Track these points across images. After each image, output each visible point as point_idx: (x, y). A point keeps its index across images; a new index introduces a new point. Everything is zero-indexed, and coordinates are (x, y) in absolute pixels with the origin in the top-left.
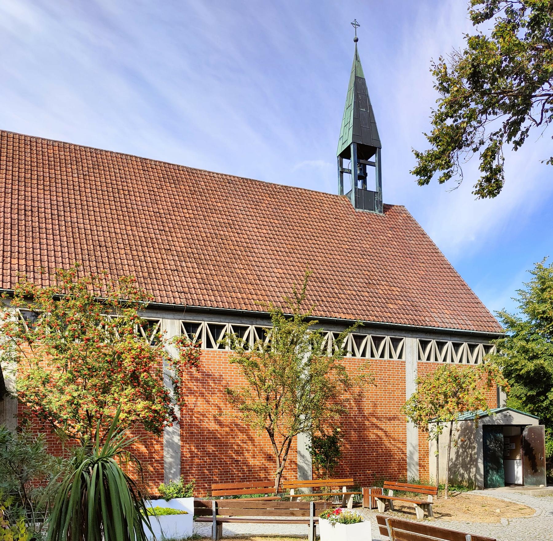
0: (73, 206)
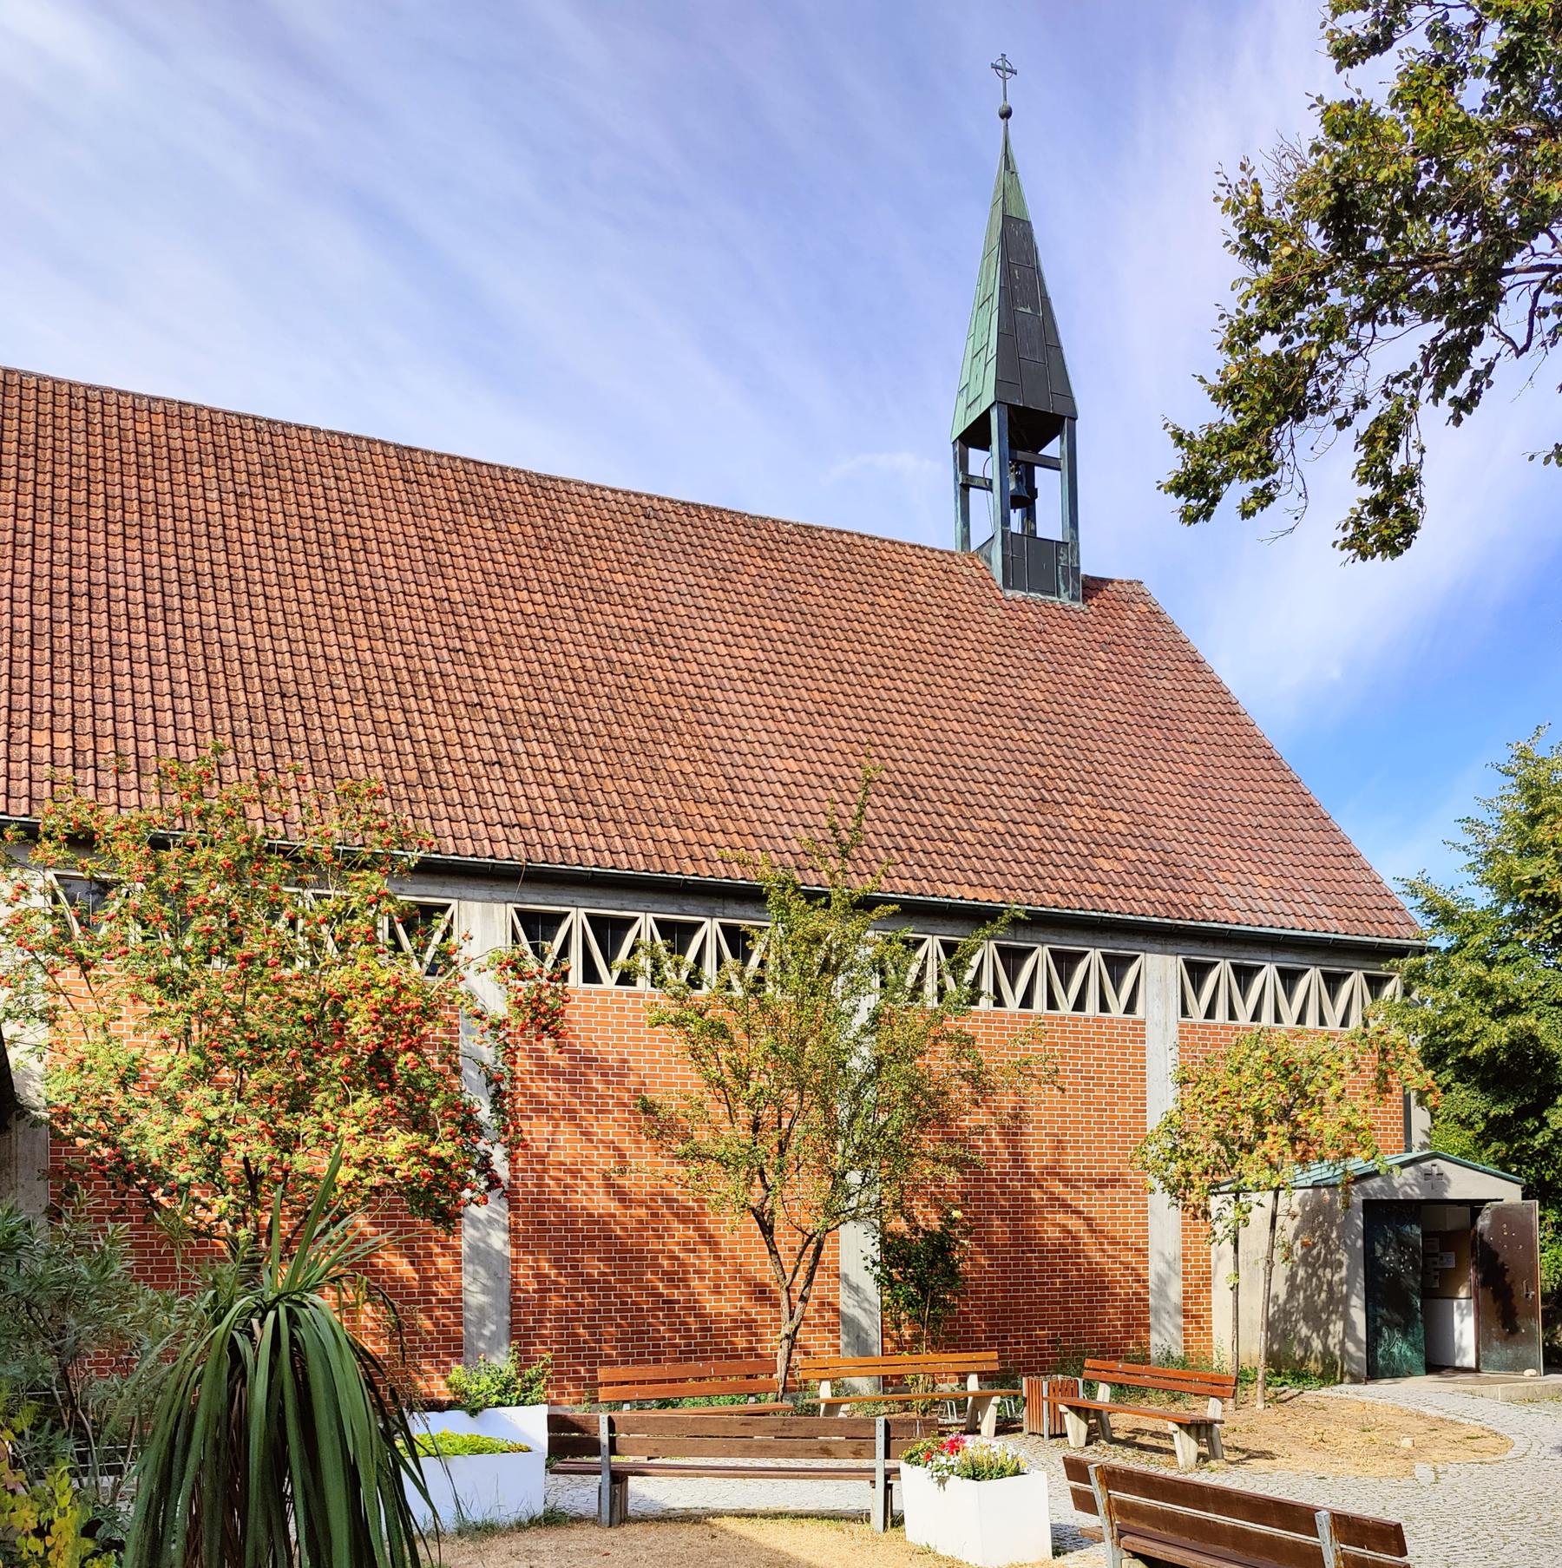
0: (207, 581)
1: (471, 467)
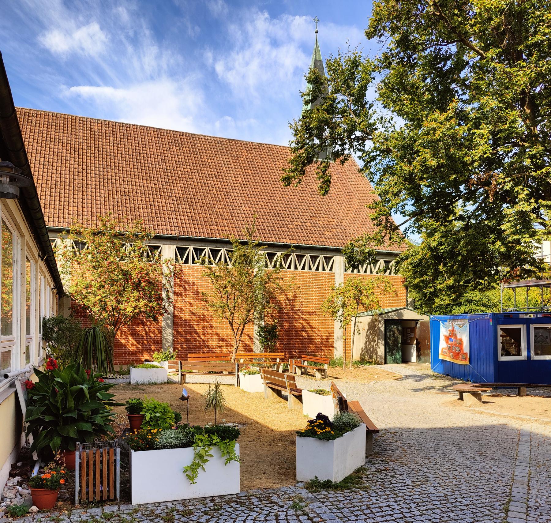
0: (109, 167)
1: (175, 133)
